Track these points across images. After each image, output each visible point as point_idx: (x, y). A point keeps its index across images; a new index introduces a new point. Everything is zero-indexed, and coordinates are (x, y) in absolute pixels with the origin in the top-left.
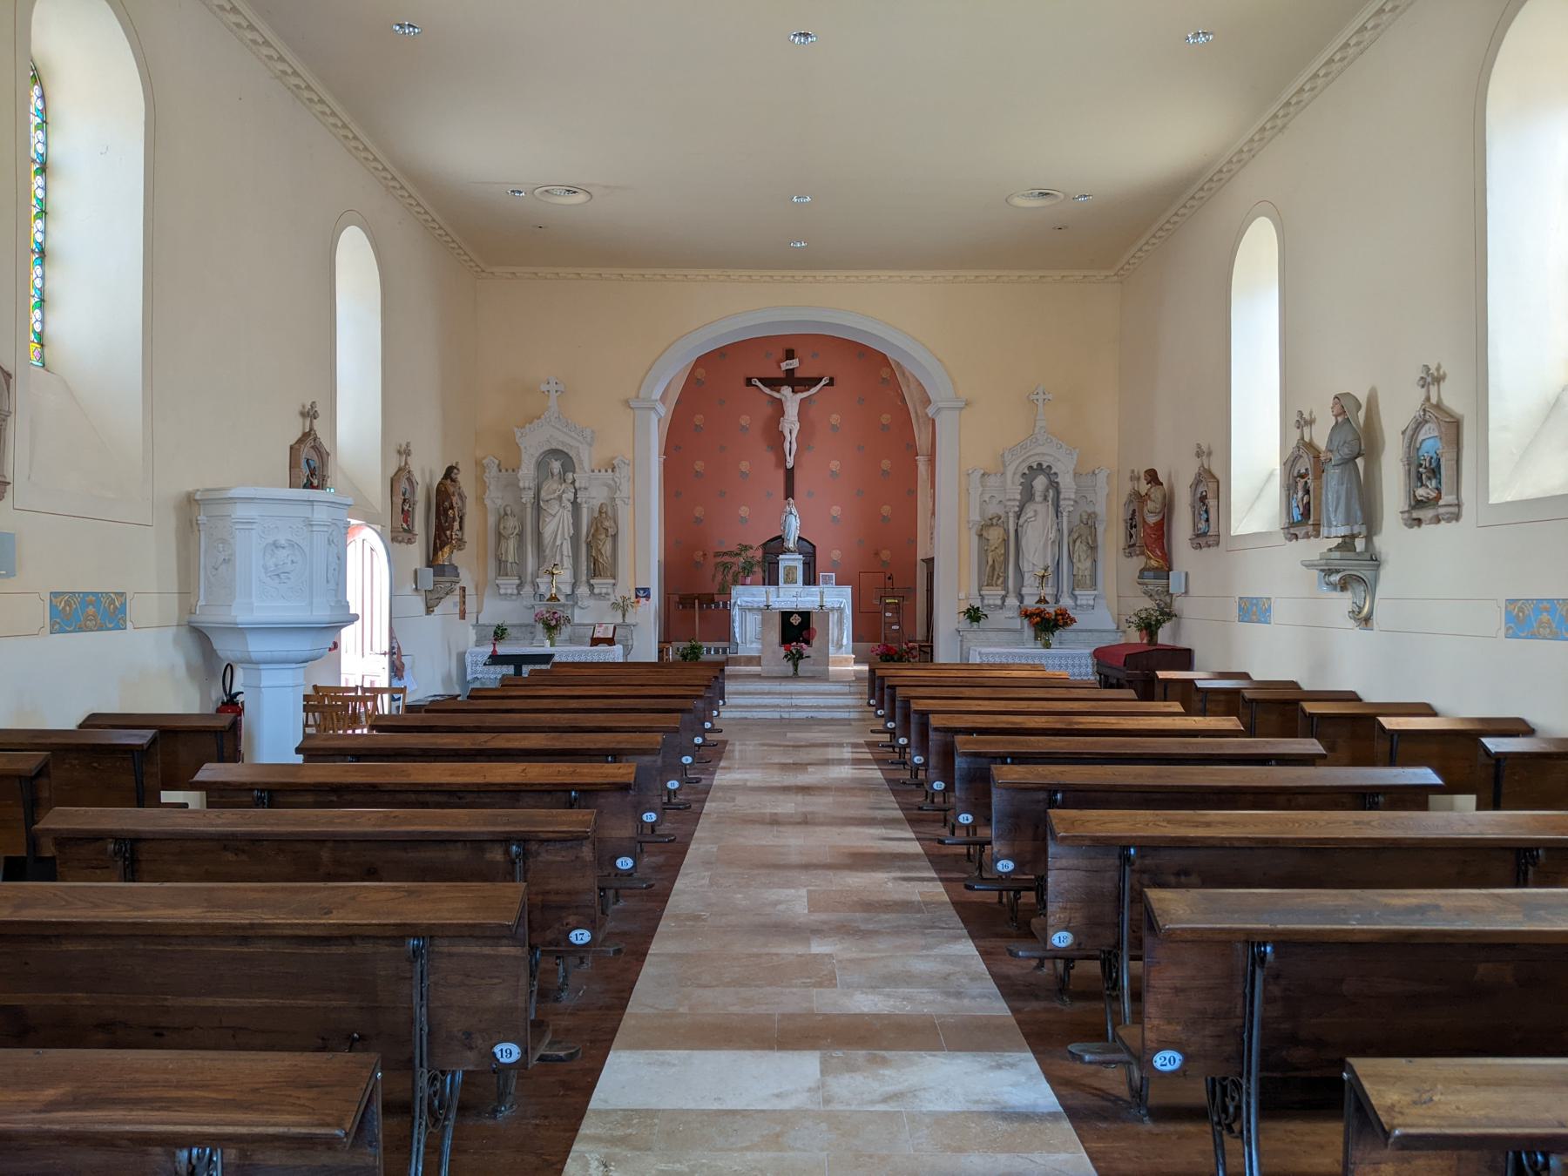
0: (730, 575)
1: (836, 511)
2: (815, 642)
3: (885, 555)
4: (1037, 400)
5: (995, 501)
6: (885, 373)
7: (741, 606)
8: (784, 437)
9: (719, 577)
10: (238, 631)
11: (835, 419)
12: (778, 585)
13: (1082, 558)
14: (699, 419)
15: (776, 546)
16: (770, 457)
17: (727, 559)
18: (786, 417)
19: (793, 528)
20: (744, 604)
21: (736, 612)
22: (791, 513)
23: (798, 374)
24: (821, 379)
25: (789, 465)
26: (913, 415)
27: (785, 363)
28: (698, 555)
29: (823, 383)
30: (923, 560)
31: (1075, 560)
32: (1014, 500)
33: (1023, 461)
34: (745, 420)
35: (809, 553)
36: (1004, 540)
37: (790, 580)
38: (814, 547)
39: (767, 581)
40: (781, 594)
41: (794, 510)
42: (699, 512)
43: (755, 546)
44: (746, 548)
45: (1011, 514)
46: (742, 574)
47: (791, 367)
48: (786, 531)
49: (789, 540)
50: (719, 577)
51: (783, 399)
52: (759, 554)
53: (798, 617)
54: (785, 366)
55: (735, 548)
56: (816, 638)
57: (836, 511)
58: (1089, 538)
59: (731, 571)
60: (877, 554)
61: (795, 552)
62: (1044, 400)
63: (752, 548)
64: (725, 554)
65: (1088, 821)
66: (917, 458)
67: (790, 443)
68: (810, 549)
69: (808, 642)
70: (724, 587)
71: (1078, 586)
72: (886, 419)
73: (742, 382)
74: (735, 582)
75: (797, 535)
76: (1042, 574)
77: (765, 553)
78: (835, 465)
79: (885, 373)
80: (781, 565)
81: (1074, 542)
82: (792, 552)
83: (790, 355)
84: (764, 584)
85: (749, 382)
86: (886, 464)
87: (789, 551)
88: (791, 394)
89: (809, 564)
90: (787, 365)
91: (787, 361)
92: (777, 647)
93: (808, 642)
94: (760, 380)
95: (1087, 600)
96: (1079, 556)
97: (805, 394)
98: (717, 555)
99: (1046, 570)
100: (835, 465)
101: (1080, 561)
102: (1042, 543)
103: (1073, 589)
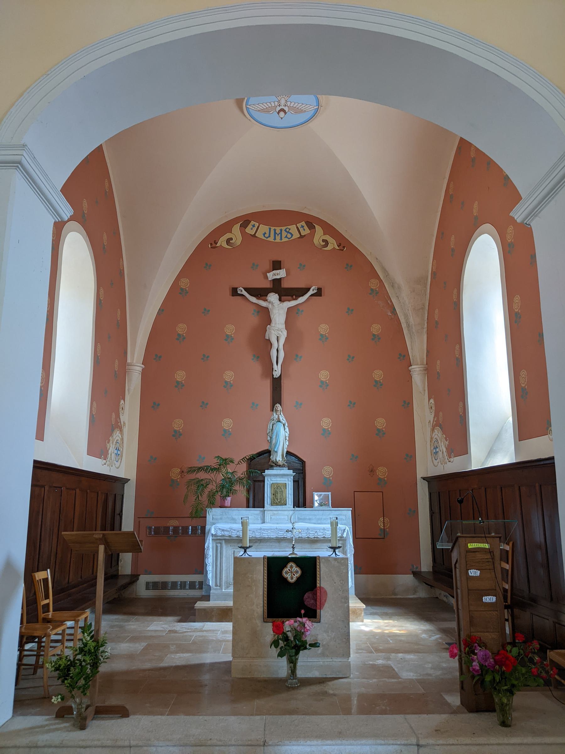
0: (205, 495)
1: (326, 423)
2: (326, 613)
3: (381, 472)
6: (373, 284)
7: (215, 535)
8: (271, 344)
9: (192, 499)
10: (300, 464)
11: (324, 329)
12: (264, 507)
14: (181, 328)
15: (322, 519)
16: (256, 368)
17: (202, 475)
18: (273, 324)
19: (281, 439)
20: (219, 533)
21: (210, 544)
22: (279, 421)
23: (285, 285)
24: (308, 290)
25: (277, 374)
26: (404, 325)
27: (272, 273)
28: (175, 473)
29: (311, 292)
30: (424, 479)
34: (230, 329)
35: (299, 469)
37: (278, 501)
38: (303, 463)
40: (267, 518)
41: (282, 418)
42: (178, 424)
43: (237, 460)
44: (225, 462)
46: (219, 493)
47: (278, 277)
48: (274, 441)
49: (276, 452)
50: (192, 499)
51: (270, 306)
52: (242, 469)
53: (295, 568)
54: (271, 276)
55: (213, 462)
56: (326, 605)
57: (326, 423)
59: (207, 491)
60: (372, 471)
61: (283, 466)
63: (232, 461)
64: (200, 469)
66: (410, 368)
67: (277, 350)
68: (298, 465)
69: (312, 614)
70: (197, 510)
72: (376, 329)
73: (228, 292)
74: (212, 504)
75: (285, 450)
77: (249, 466)
78: (324, 375)
79: (373, 284)
80: (268, 482)
82: (280, 466)
83: (277, 265)
84: (248, 507)
85: (234, 292)
86: (378, 375)
87: (277, 465)
88: (278, 302)
89: (298, 481)
90: (274, 275)
91: (274, 272)
92: (259, 622)
93: (312, 614)
94: (246, 289)
97: (293, 303)
98: (192, 470)
100: (324, 375)
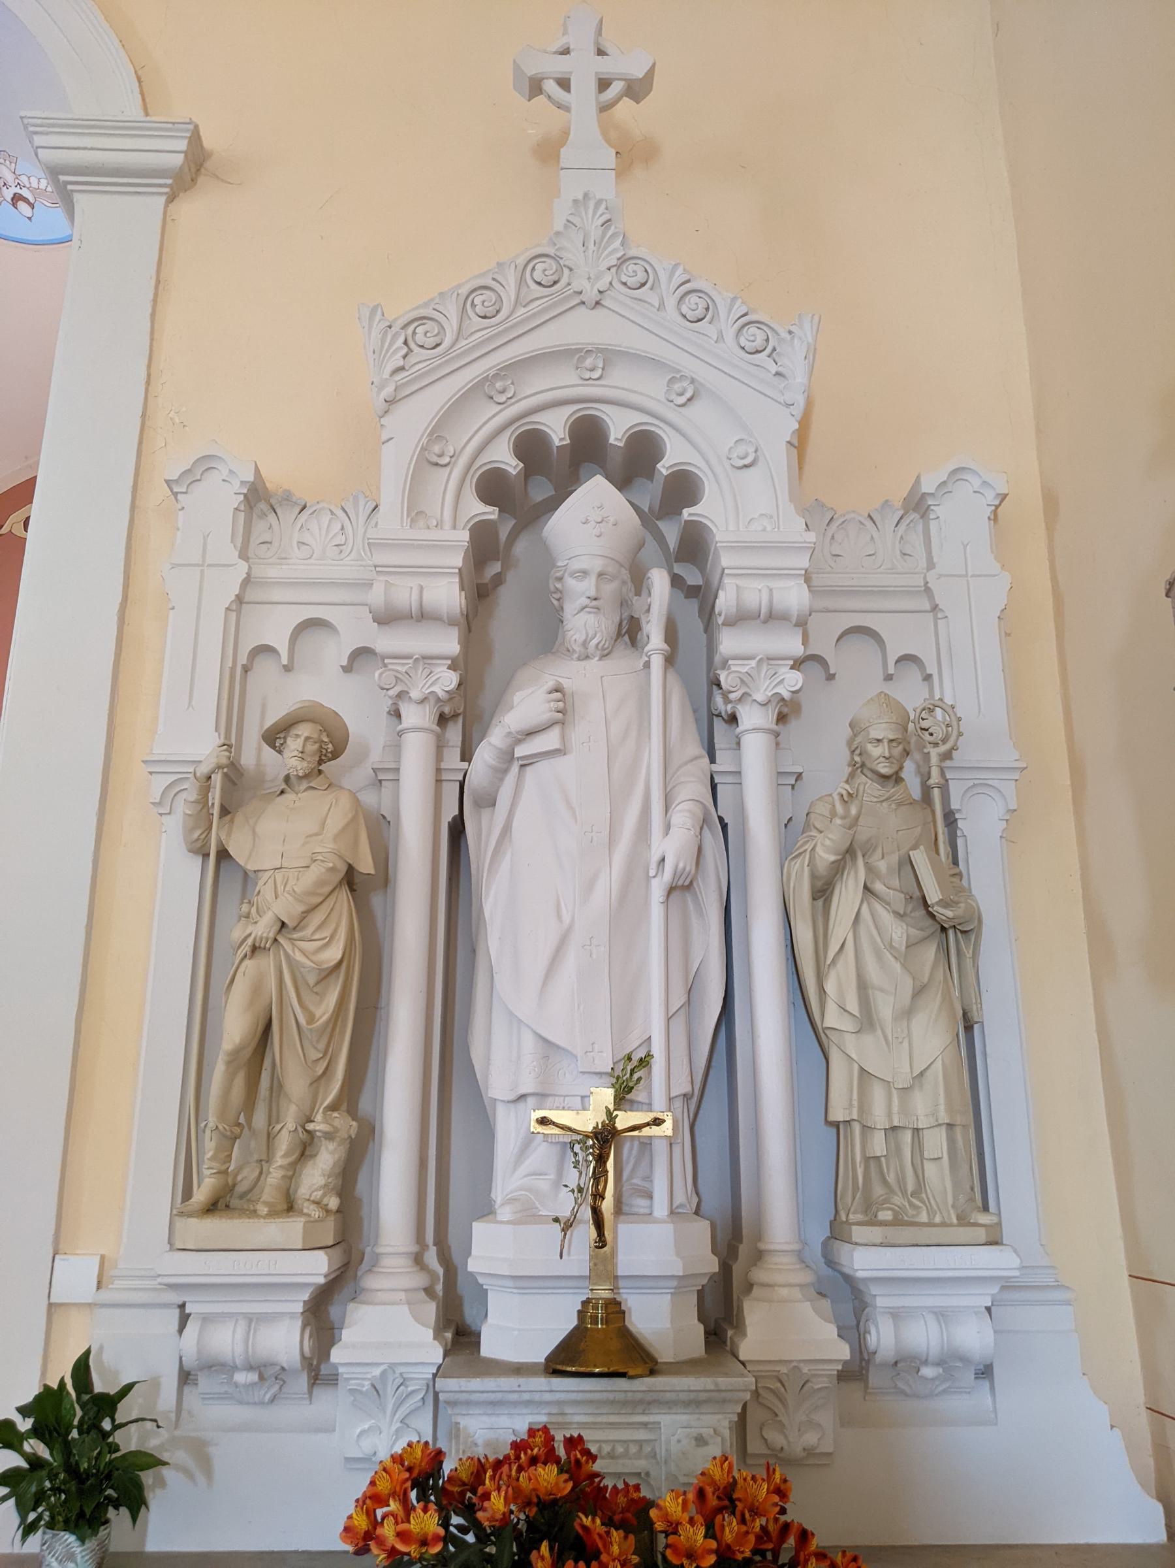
4: (564, 84)
5: (335, 652)
13: (885, 1008)
31: (832, 1019)
32: (423, 616)
33: (483, 389)
36: (350, 879)
39: (335, 1377)
45: (416, 717)
58: (920, 858)
62: (604, 84)
65: (925, 1322)
71: (870, 1210)
76: (588, 1121)
81: (823, 892)
95: (941, 1315)
96: (863, 986)
99: (623, 1095)
101: (867, 1020)
102: (601, 897)
103: (838, 1232)
